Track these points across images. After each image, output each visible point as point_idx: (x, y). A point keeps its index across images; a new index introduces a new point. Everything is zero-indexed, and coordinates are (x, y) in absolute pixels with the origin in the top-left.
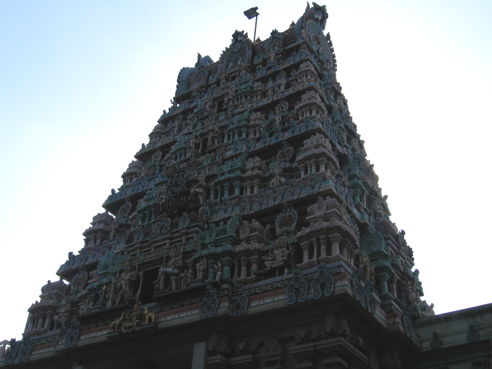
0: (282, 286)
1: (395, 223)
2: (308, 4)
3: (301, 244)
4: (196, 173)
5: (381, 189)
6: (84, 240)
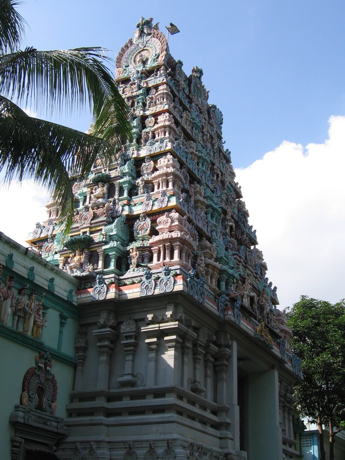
1: (261, 251)
3: (152, 249)
4: (107, 170)
5: (248, 211)
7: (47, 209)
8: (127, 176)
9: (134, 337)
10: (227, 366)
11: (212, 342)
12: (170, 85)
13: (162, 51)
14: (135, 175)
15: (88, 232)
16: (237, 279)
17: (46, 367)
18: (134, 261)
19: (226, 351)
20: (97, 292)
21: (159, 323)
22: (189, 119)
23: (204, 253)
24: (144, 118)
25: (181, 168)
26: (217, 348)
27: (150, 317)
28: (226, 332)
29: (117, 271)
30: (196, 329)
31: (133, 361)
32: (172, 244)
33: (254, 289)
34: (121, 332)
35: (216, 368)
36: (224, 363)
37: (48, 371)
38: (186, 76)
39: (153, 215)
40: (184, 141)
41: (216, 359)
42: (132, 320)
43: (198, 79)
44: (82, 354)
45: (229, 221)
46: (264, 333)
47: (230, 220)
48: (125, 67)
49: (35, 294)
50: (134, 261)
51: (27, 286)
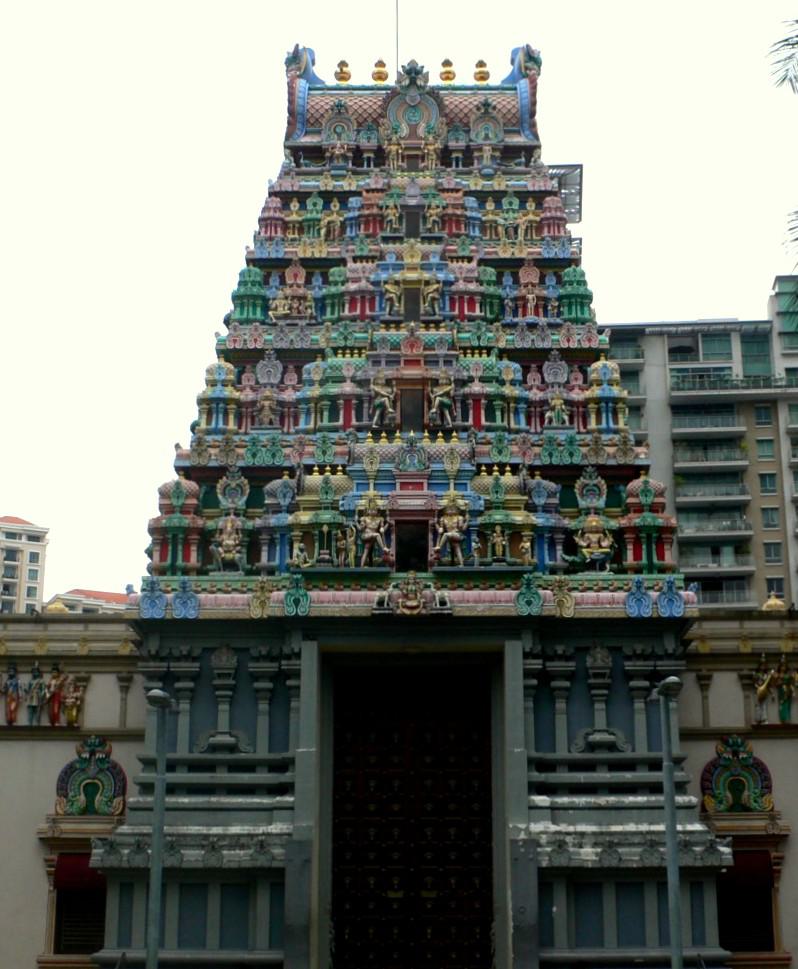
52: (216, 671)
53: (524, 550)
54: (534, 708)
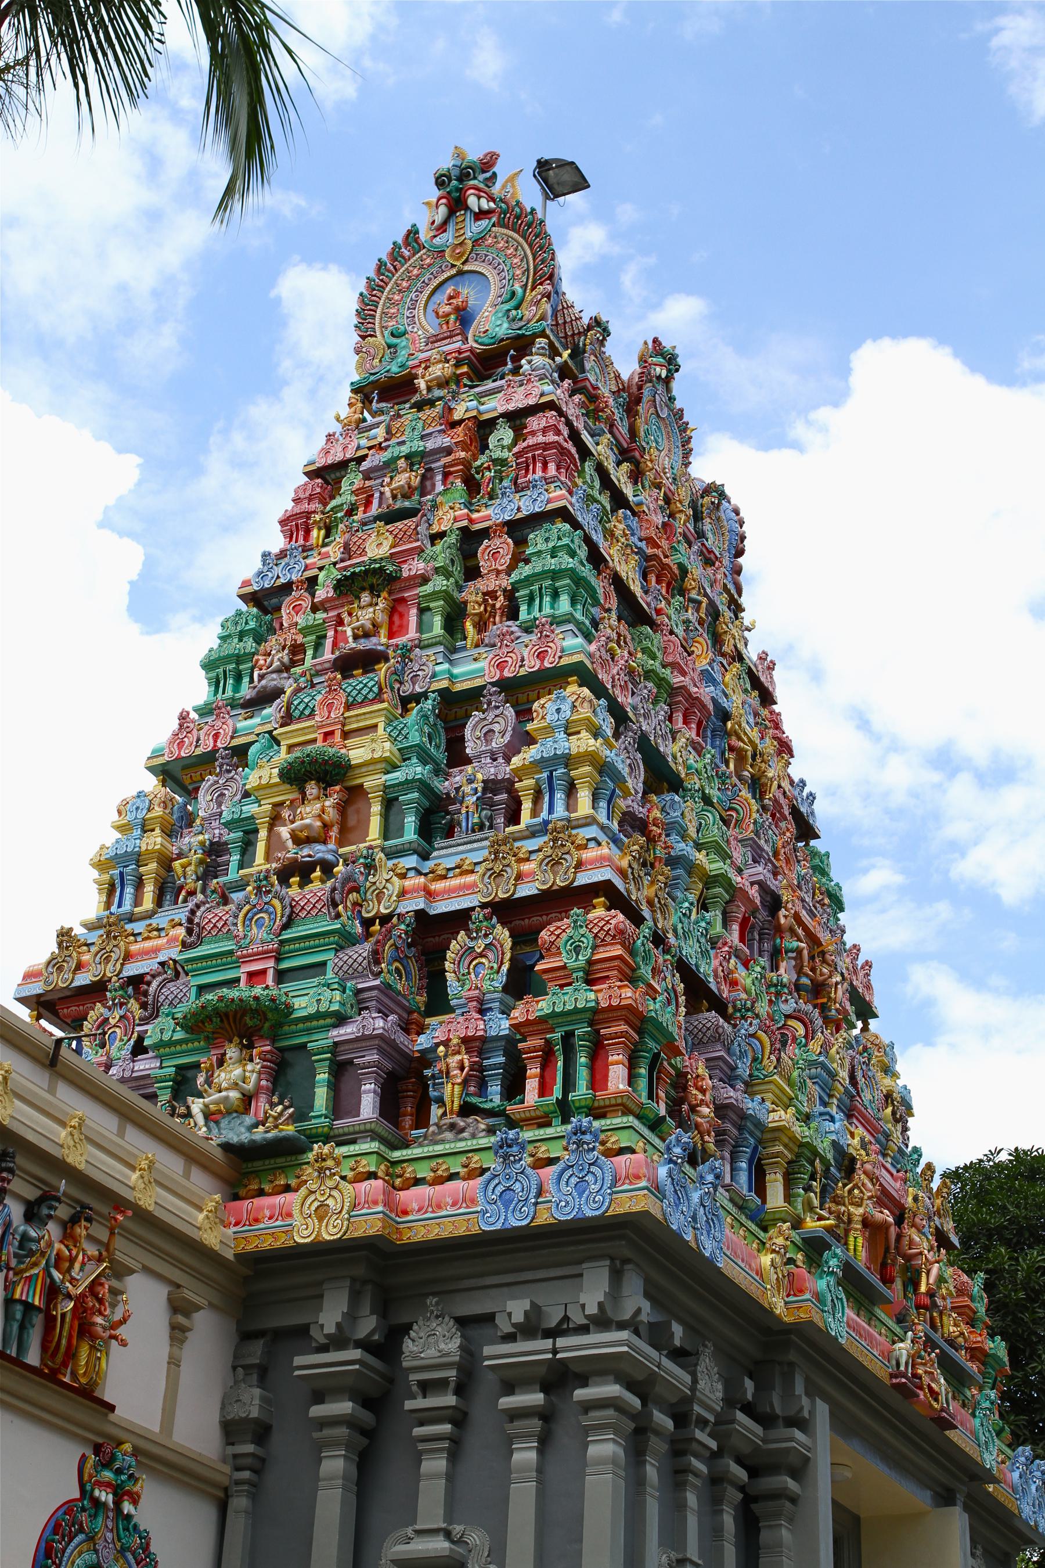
0: (463, 1171)
2: (646, 343)
6: (138, 465)
7: (95, 874)
8: (415, 760)
9: (452, 1385)
10: (794, 1500)
11: (739, 1406)
12: (569, 413)
13: (534, 281)
14: (442, 757)
15: (271, 973)
16: (824, 1160)
17: (118, 1503)
18: (452, 1092)
19: (792, 1439)
20: (313, 1208)
21: (552, 1333)
22: (635, 539)
23: (707, 1060)
24: (470, 539)
25: (617, 735)
26: (759, 1430)
27: (517, 1309)
28: (791, 1364)
29: (384, 1128)
30: (679, 1355)
31: (450, 1477)
32: (598, 1031)
33: (885, 1199)
34: (405, 1364)
35: (753, 1506)
36: (787, 1488)
37: (128, 1517)
38: (618, 377)
39: (524, 917)
40: (623, 628)
41: (754, 1472)
42: (447, 1319)
43: (660, 388)
44: (250, 1448)
45: (787, 935)
46: (922, 1367)
47: (792, 931)
48: (393, 335)
49: (89, 1220)
50: (452, 1092)
51: (58, 1190)
52: (414, 1377)
53: (275, 1099)
54: (540, 1470)
